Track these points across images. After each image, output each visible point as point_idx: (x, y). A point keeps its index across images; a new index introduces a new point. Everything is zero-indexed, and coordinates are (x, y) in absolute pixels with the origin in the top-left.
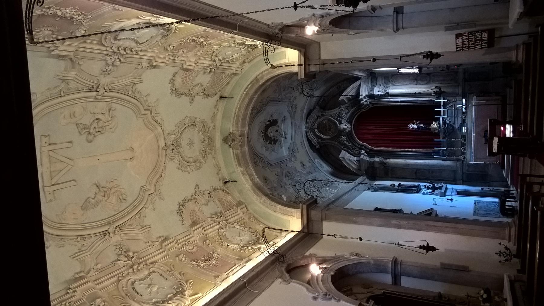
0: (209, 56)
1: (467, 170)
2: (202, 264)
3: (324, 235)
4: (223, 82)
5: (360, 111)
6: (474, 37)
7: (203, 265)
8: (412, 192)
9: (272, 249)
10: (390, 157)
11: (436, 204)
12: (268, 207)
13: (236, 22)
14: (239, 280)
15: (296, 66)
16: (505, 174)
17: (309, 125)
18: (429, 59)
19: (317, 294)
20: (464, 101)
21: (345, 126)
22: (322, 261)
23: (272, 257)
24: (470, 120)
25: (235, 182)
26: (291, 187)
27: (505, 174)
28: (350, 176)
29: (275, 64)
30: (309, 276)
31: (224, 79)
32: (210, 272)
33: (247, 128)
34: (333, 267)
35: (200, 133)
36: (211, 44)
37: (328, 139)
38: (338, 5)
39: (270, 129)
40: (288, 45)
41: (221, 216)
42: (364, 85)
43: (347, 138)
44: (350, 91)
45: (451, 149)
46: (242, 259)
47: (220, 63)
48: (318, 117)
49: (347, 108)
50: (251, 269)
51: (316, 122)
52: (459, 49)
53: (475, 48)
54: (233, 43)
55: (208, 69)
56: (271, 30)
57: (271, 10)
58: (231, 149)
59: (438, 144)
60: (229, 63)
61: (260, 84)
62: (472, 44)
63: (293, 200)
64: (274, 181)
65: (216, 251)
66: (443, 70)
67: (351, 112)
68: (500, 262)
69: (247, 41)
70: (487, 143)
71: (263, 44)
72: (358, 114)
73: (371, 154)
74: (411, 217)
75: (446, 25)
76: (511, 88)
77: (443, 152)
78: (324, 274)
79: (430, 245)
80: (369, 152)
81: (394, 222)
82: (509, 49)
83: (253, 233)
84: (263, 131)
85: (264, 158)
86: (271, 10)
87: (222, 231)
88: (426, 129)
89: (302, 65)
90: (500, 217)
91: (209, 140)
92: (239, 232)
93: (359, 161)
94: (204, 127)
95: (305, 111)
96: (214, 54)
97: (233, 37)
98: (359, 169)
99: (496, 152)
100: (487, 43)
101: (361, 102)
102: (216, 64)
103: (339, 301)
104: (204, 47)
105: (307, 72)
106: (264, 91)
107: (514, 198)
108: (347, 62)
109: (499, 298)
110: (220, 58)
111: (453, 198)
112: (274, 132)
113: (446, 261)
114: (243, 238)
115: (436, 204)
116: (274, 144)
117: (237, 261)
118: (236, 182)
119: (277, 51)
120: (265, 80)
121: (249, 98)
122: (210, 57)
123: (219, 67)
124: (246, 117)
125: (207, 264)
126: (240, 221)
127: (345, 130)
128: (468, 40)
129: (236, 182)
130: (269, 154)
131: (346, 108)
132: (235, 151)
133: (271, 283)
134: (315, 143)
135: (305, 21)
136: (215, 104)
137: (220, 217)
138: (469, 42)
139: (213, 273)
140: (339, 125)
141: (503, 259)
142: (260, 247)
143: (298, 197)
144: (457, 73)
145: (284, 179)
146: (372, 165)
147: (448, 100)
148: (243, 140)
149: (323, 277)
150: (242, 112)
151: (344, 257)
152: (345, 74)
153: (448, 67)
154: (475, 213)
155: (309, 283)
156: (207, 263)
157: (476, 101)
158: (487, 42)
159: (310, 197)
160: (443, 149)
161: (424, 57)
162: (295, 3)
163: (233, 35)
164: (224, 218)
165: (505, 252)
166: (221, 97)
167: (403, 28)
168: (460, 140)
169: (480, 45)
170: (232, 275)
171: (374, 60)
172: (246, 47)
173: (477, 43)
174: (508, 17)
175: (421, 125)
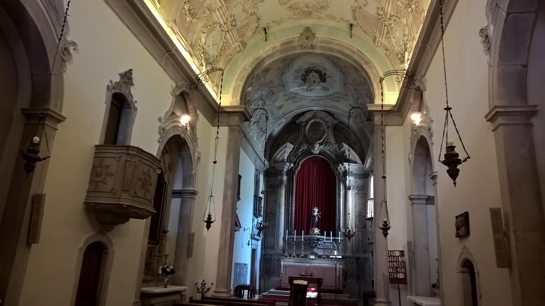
0: (395, 13)
1: (274, 259)
2: (187, 7)
3: (218, 128)
4: (367, 28)
5: (332, 163)
6: (400, 266)
7: (186, 8)
8: (255, 209)
9: (202, 78)
10: (287, 190)
11: (244, 230)
12: (241, 73)
13: (429, 44)
14: (174, 45)
15: (382, 102)
16: (272, 290)
17: (319, 114)
18: (382, 227)
19: (164, 121)
20: (340, 257)
21: (317, 148)
22: (193, 125)
23: (195, 77)
24: (321, 262)
25: (266, 39)
26: (259, 95)
27: (272, 290)
28: (268, 152)
29: (384, 82)
30: (178, 114)
31: (370, 29)
32: (180, 16)
33: (319, 52)
34: (187, 136)
35: (316, 3)
36: (408, 15)
37: (305, 131)
38: (447, 147)
39: (317, 75)
40: (402, 95)
41: (232, 26)
42: (357, 167)
43: (305, 151)
44: (352, 155)
45: (294, 245)
46: (192, 47)
47: (387, 25)
48: (327, 122)
49: (335, 150)
50: (184, 57)
51: (322, 121)
52: (390, 253)
53: (390, 267)
54: (408, 39)
55: (382, 12)
56: (419, 78)
57: (446, 86)
58: (298, 35)
59: (299, 234)
60: (387, 34)
61: (364, 66)
62: (394, 264)
63: (247, 98)
64: (265, 78)
65: (199, 21)
66: (368, 239)
67: (331, 154)
68: (196, 284)
69: (409, 54)
70: (300, 276)
71: (405, 70)
72: (329, 161)
73: (290, 173)
74: (234, 208)
75: (412, 242)
76: (350, 298)
77: (291, 238)
78: (182, 128)
79: (212, 224)
80: (291, 171)
81: (229, 193)
82: (387, 296)
83: (216, 58)
84: (315, 67)
85: (288, 69)
86: (446, 86)
87: (218, 27)
88: (313, 223)
89: (382, 108)
90: (234, 285)
91: (308, 13)
92: (217, 44)
93: (283, 161)
94: (322, 8)
95: (333, 110)
96: (397, 19)
97: (414, 39)
98: (275, 162)
99: (294, 283)
100: (394, 277)
101: (340, 164)
102: (387, 20)
103: (159, 142)
104: (406, 8)
105: (374, 113)
106: (356, 69)
107: (251, 297)
108: (383, 153)
109: (167, 281)
110: (393, 25)
111: (250, 245)
112: (314, 79)
113: (196, 237)
114: (211, 49)
115: (244, 230)
116: (302, 78)
117: (190, 43)
118: (266, 41)
119: (396, 83)
120: (367, 71)
121: (350, 55)
122: (394, 14)
123: (383, 24)
124: (331, 51)
125: (187, 12)
126: (227, 44)
127: (313, 148)
128: (397, 261)
129: (266, 41)
130: (292, 74)
131: (334, 150)
132: (296, 40)
133: (171, 77)
134: (301, 119)
135: (426, 112)
136: (345, 19)
137: (231, 25)
138: (396, 262)
139: (178, 20)
140: (319, 143)
141: (199, 286)
142: (203, 65)
143: (250, 103)
144: (365, 252)
145: (267, 89)
146: (280, 173)
147: (340, 243)
148: (307, 49)
149: (178, 127)
150: (336, 47)
151: (196, 147)
152: (369, 147)
153: (371, 244)
154: (237, 264)
155: (173, 113)
156: (187, 12)
157: (339, 268)
158: (395, 277)
159: (252, 114)
160: (294, 238)
161: (385, 222)
162: (451, 108)
163: (417, 40)
164: (230, 29)
165: (205, 288)
166: (351, 25)
167: (412, 204)
168: (303, 253)
169: (392, 272)
170: (177, 38)
171: (384, 178)
172: (402, 51)
173: (395, 269)
174: (417, 295)
175: (317, 219)
